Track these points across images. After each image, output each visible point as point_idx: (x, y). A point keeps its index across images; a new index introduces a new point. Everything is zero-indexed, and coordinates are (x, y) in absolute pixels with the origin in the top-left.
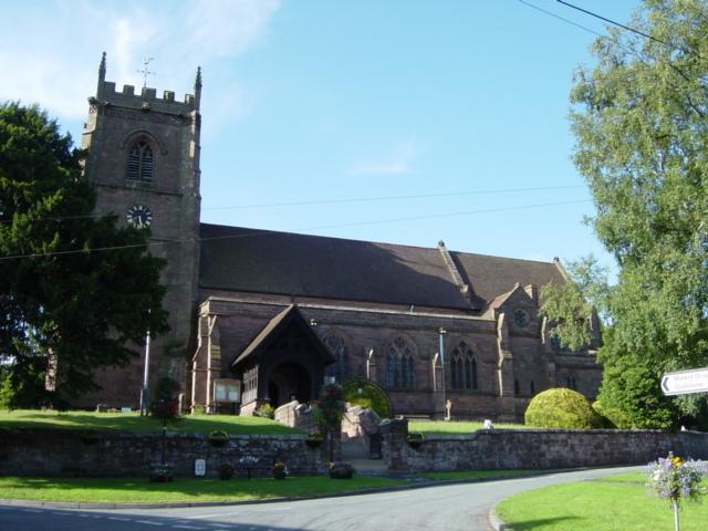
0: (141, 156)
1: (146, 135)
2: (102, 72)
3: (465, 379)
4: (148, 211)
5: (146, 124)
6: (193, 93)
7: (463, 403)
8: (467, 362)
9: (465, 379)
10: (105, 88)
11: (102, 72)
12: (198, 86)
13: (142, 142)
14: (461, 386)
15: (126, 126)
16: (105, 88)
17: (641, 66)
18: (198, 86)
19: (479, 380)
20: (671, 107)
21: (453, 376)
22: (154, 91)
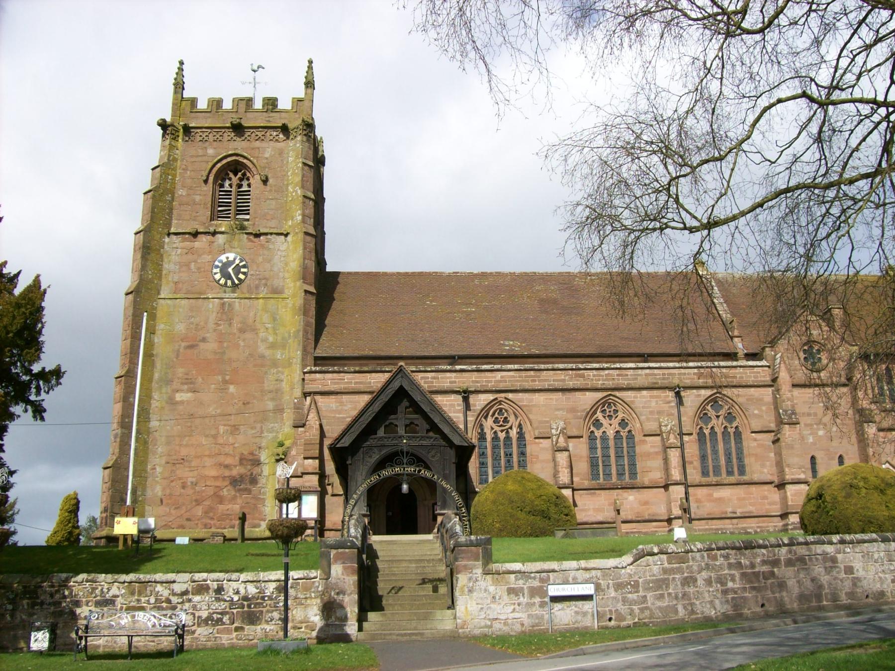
0: (234, 189)
1: (241, 159)
2: (179, 86)
3: (721, 447)
4: (244, 266)
5: (238, 146)
6: (301, 93)
7: (720, 499)
8: (725, 432)
9: (721, 447)
10: (183, 102)
11: (179, 86)
12: (310, 84)
13: (235, 167)
14: (717, 471)
15: (210, 151)
16: (183, 102)
17: (65, 597)
18: (310, 84)
19: (747, 461)
20: (698, 607)
21: (603, 651)
22: (164, 120)
